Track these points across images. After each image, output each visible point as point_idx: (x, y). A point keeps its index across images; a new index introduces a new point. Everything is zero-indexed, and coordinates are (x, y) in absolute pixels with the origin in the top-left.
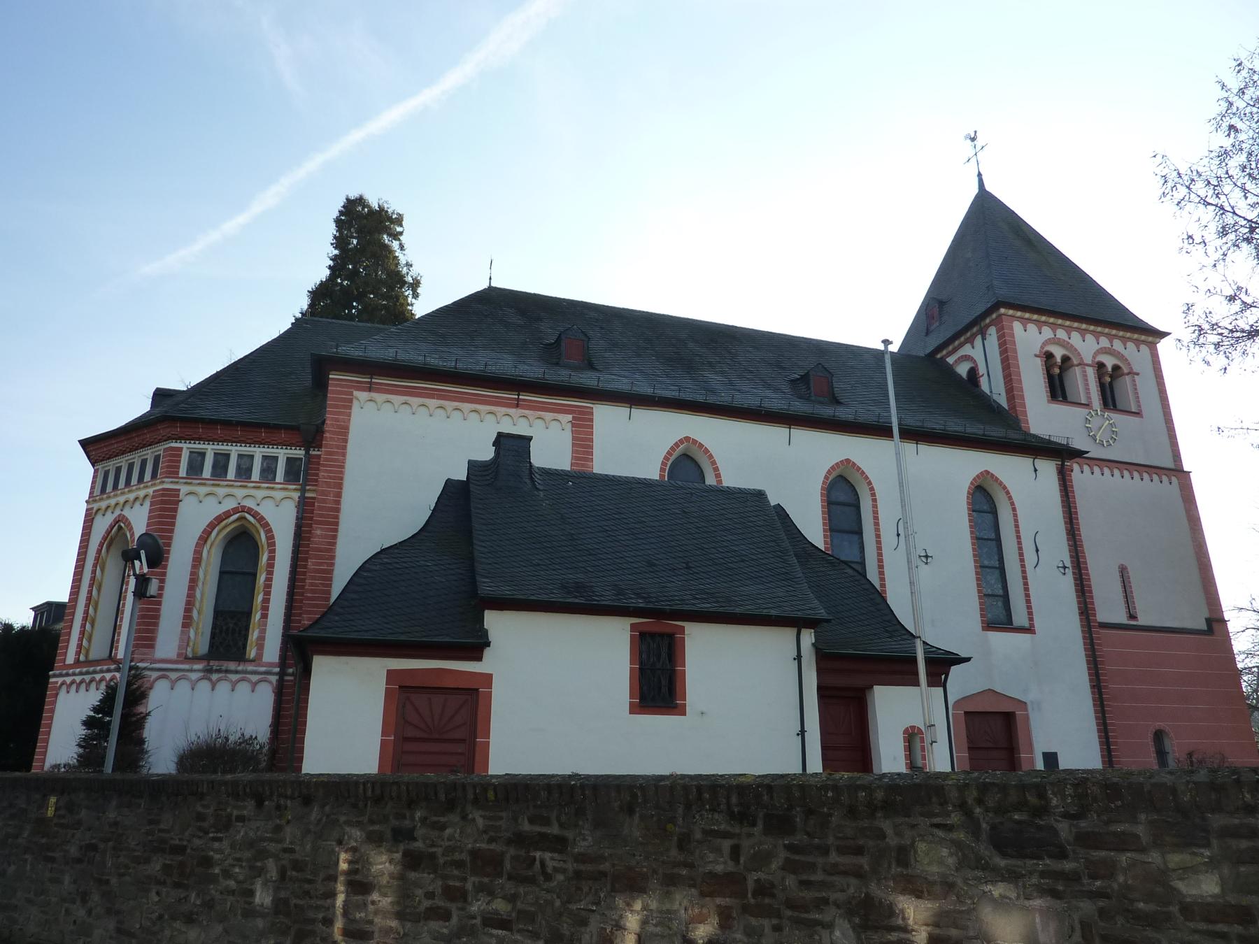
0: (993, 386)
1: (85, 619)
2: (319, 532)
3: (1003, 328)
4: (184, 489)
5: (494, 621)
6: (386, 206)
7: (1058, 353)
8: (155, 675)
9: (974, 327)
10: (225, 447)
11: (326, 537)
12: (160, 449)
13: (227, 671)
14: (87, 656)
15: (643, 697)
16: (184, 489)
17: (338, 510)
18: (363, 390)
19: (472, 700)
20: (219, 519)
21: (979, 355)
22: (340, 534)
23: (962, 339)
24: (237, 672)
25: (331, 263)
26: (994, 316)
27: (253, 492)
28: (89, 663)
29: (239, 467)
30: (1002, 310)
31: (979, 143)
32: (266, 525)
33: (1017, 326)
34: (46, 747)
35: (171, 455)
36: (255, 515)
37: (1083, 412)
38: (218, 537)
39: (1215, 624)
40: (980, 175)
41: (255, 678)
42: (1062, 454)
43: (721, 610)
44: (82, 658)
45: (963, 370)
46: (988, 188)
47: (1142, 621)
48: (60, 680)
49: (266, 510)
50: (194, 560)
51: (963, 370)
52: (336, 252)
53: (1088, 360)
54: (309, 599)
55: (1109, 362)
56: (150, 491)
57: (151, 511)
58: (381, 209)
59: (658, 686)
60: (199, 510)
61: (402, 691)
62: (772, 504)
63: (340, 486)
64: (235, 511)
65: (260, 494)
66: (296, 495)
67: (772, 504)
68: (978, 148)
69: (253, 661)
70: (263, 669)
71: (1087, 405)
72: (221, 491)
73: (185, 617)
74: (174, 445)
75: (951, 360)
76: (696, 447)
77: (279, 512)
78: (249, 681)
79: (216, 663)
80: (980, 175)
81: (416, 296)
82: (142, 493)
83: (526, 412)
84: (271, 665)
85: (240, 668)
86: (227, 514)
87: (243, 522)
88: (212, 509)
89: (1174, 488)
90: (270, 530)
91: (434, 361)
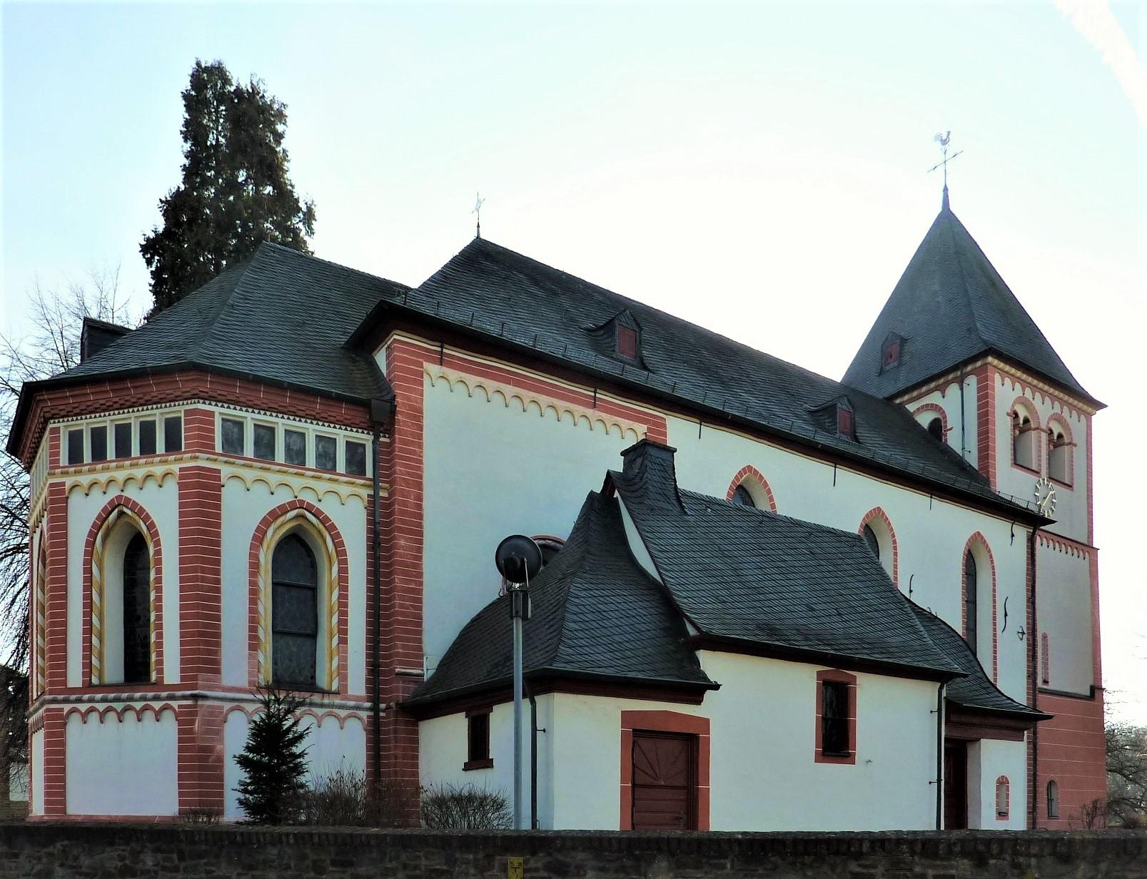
0: (962, 440)
2: (402, 542)
3: (986, 379)
4: (69, 481)
5: (712, 663)
6: (262, 87)
7: (1023, 413)
8: (227, 706)
9: (954, 371)
10: (268, 418)
11: (411, 549)
12: (178, 410)
13: (312, 704)
14: (100, 677)
15: (825, 749)
16: (226, 471)
17: (420, 516)
18: (433, 361)
19: (691, 744)
20: (274, 515)
21: (952, 406)
22: (426, 546)
23: (933, 385)
24: (322, 706)
25: (187, 162)
26: (979, 364)
27: (312, 483)
29: (288, 449)
30: (990, 359)
31: (952, 147)
32: (331, 528)
33: (997, 377)
36: (317, 514)
37: (1032, 478)
38: (273, 536)
39: (1096, 691)
40: (946, 189)
41: (343, 713)
42: (1032, 520)
43: (915, 664)
44: (95, 681)
45: (925, 420)
46: (954, 208)
47: (1051, 687)
49: (329, 507)
51: (925, 420)
53: (1043, 426)
54: (399, 622)
55: (1057, 429)
58: (254, 92)
59: (836, 740)
61: (639, 737)
63: (419, 486)
64: (293, 505)
65: (139, 473)
66: (365, 493)
68: (950, 154)
69: (337, 693)
70: (352, 703)
71: (1037, 473)
72: (103, 477)
73: (251, 638)
74: (201, 406)
75: (911, 407)
76: (756, 479)
77: (346, 510)
78: (115, 710)
79: (296, 694)
80: (946, 189)
81: (311, 232)
83: (604, 416)
84: (357, 698)
85: (326, 701)
86: (283, 510)
87: (301, 521)
88: (98, 502)
89: (1085, 564)
90: (338, 535)
91: (491, 327)
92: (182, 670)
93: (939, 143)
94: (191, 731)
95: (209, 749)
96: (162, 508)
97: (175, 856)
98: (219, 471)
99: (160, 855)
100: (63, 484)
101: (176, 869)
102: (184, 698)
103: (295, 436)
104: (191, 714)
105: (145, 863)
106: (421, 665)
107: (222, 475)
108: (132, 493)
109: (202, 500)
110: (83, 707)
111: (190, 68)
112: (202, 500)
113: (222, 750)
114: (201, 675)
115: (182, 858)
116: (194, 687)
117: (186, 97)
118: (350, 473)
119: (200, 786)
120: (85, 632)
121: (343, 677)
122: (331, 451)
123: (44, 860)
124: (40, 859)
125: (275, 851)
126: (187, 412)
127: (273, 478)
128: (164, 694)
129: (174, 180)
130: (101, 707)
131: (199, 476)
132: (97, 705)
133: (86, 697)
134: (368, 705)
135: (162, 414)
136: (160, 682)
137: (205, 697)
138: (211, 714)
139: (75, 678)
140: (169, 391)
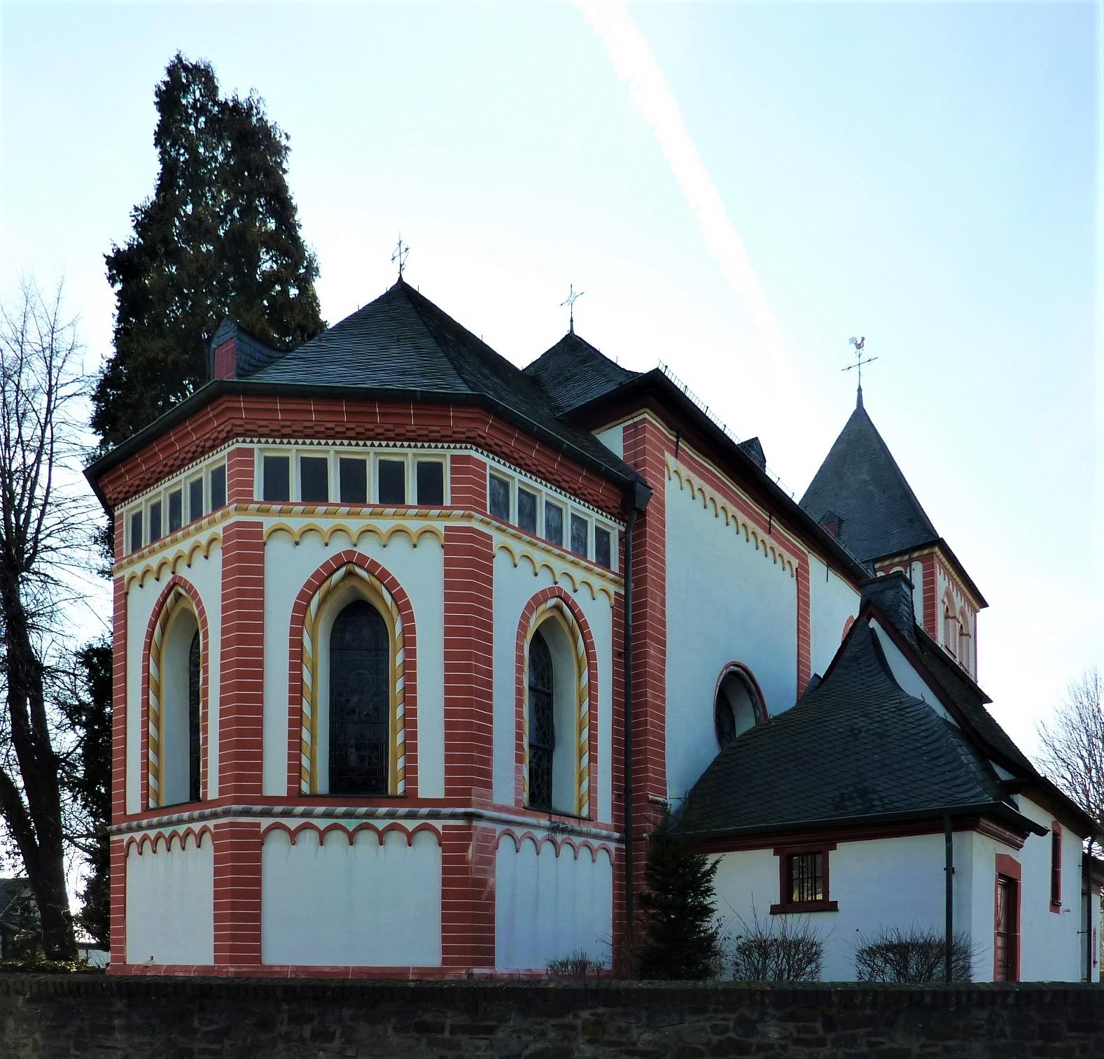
1: (145, 746)
4: (268, 523)
8: (499, 829)
12: (219, 457)
14: (312, 784)
16: (268, 523)
24: (580, 834)
26: (926, 552)
28: (159, 810)
31: (866, 353)
34: (124, 900)
35: (240, 463)
40: (860, 390)
44: (305, 788)
46: (867, 406)
48: (126, 837)
49: (582, 599)
50: (292, 689)
52: (168, 79)
56: (218, 530)
57: (225, 563)
60: (289, 569)
62: (838, 844)
65: (384, 526)
67: (838, 844)
80: (860, 390)
82: (203, 538)
84: (606, 827)
87: (353, 582)
88: (314, 556)
92: (447, 781)
93: (854, 346)
94: (463, 860)
95: (482, 883)
96: (207, 580)
97: (818, 1025)
98: (490, 538)
99: (791, 1026)
100: (260, 525)
101: (821, 1043)
102: (453, 816)
103: (553, 510)
104: (462, 837)
105: (765, 1035)
106: (664, 793)
107: (494, 543)
108: (369, 549)
109: (468, 572)
110: (292, 823)
111: (167, 60)
112: (468, 572)
113: (494, 885)
114: (475, 789)
115: (829, 1025)
116: (467, 803)
117: (159, 93)
118: (598, 564)
119: (472, 929)
120: (291, 723)
121: (593, 801)
122: (583, 535)
123: (552, 1035)
124: (543, 1034)
125: (984, 1014)
126: (454, 459)
127: (326, 524)
128: (208, 811)
129: (145, 190)
130: (322, 824)
131: (471, 539)
132: (315, 822)
133: (144, 822)
134: (617, 835)
135: (415, 455)
136: (410, 797)
137: (480, 817)
138: (485, 838)
139: (275, 782)
140: (435, 427)
